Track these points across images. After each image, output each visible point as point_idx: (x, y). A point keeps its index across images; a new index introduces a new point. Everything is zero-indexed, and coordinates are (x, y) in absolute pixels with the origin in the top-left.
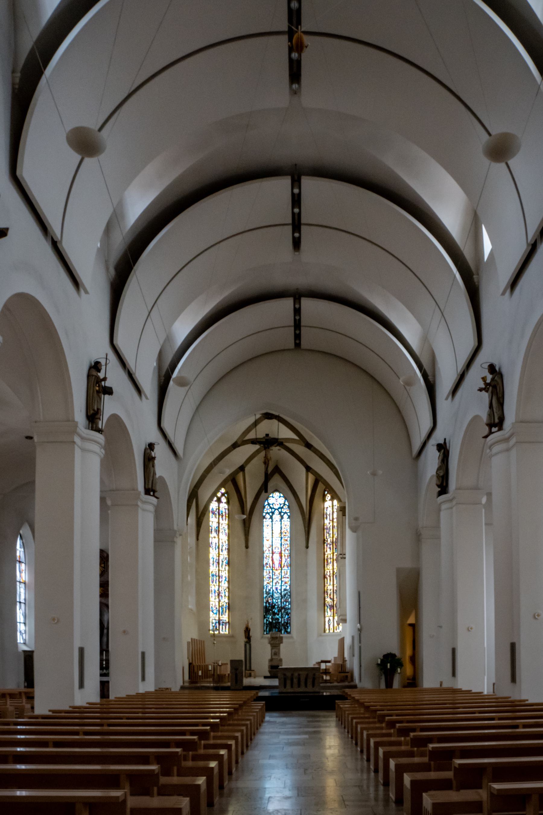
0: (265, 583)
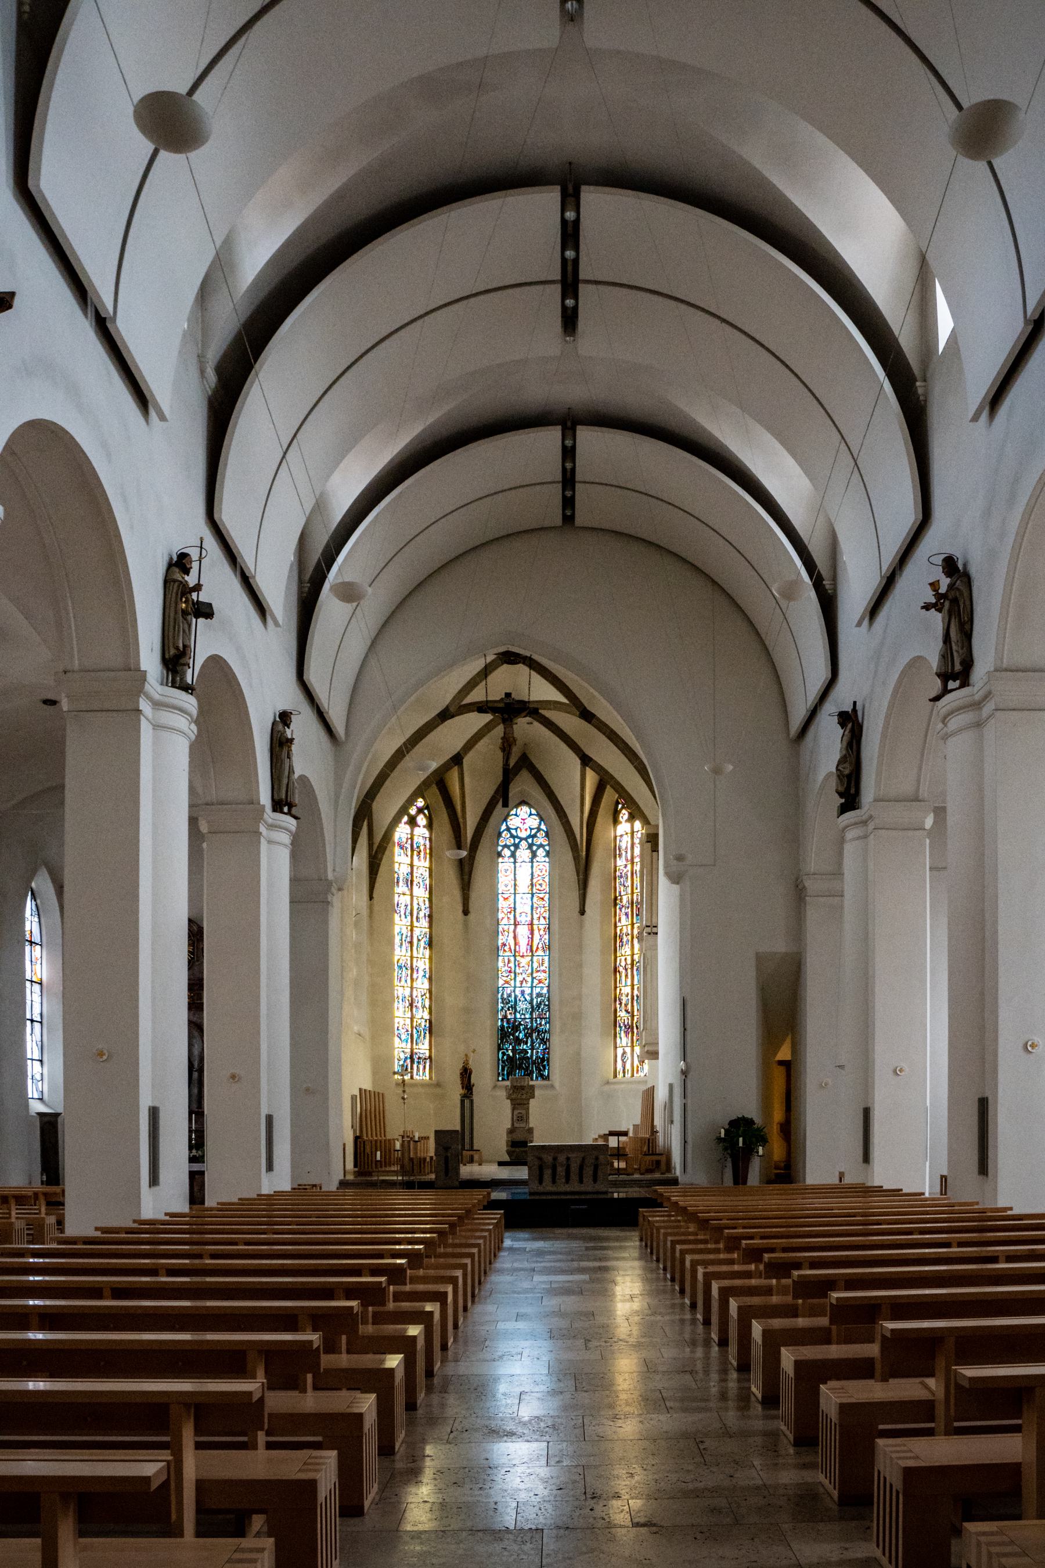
0: (501, 982)
